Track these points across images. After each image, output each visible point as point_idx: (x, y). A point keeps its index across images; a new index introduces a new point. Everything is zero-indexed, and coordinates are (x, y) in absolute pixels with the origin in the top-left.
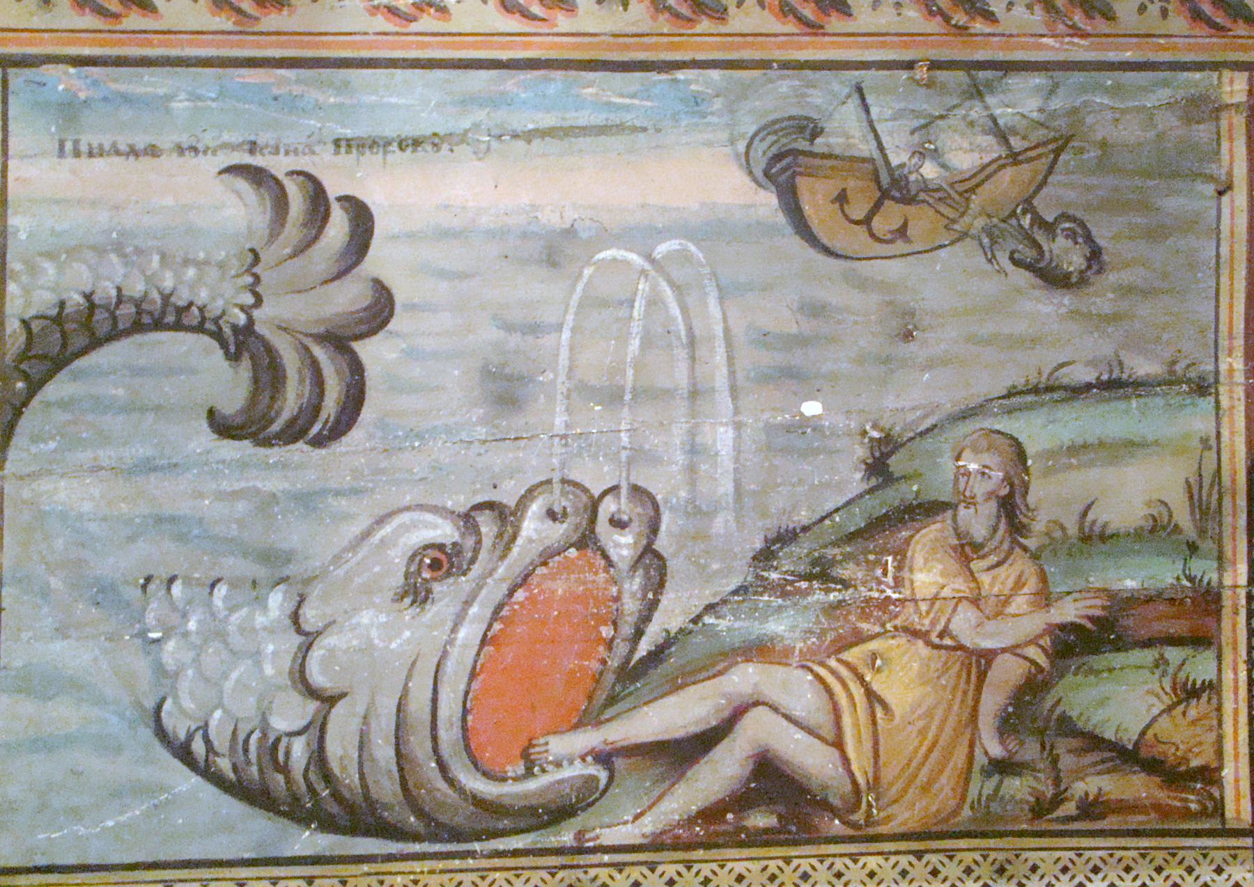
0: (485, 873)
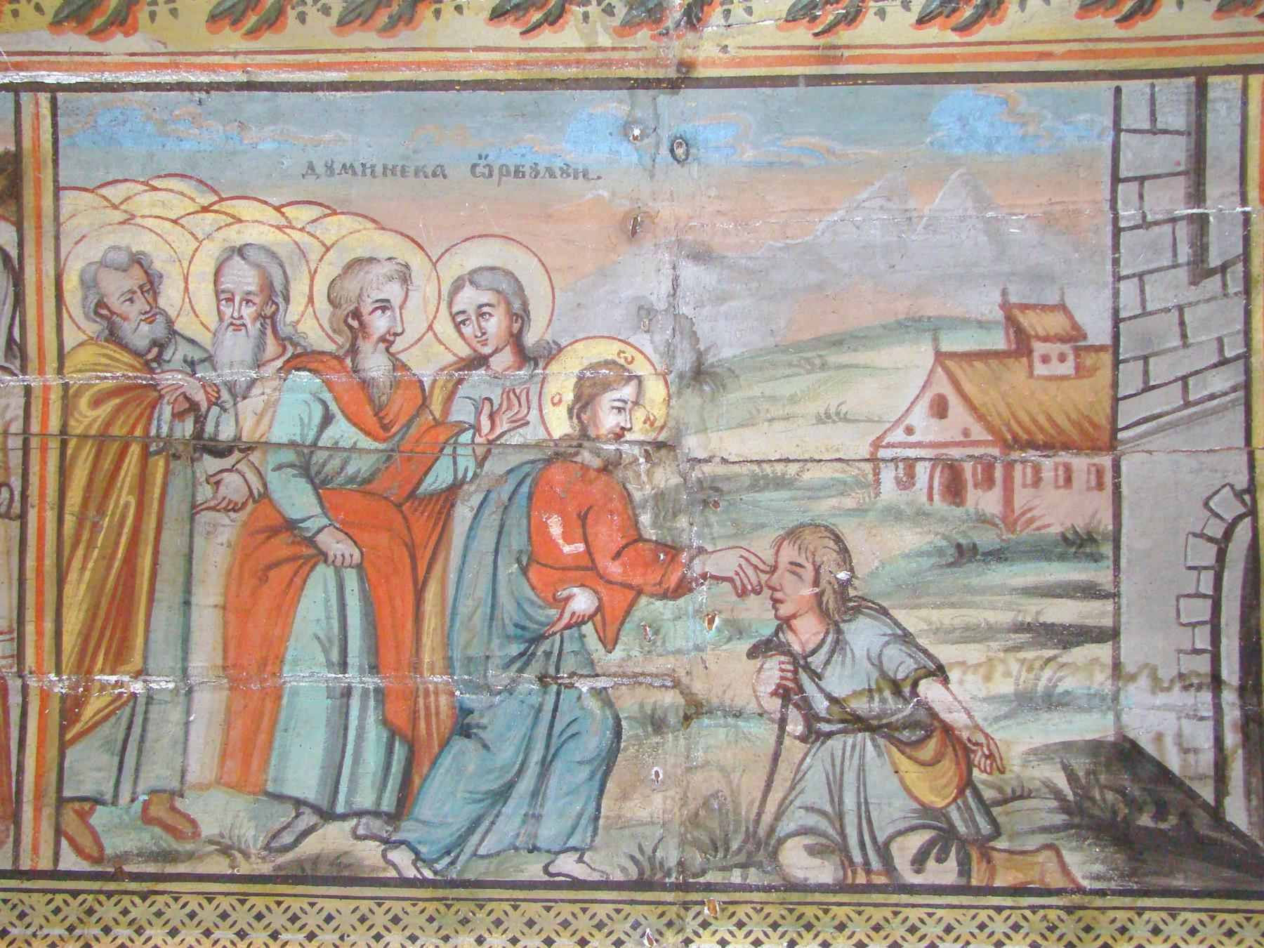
0: (620, 906)
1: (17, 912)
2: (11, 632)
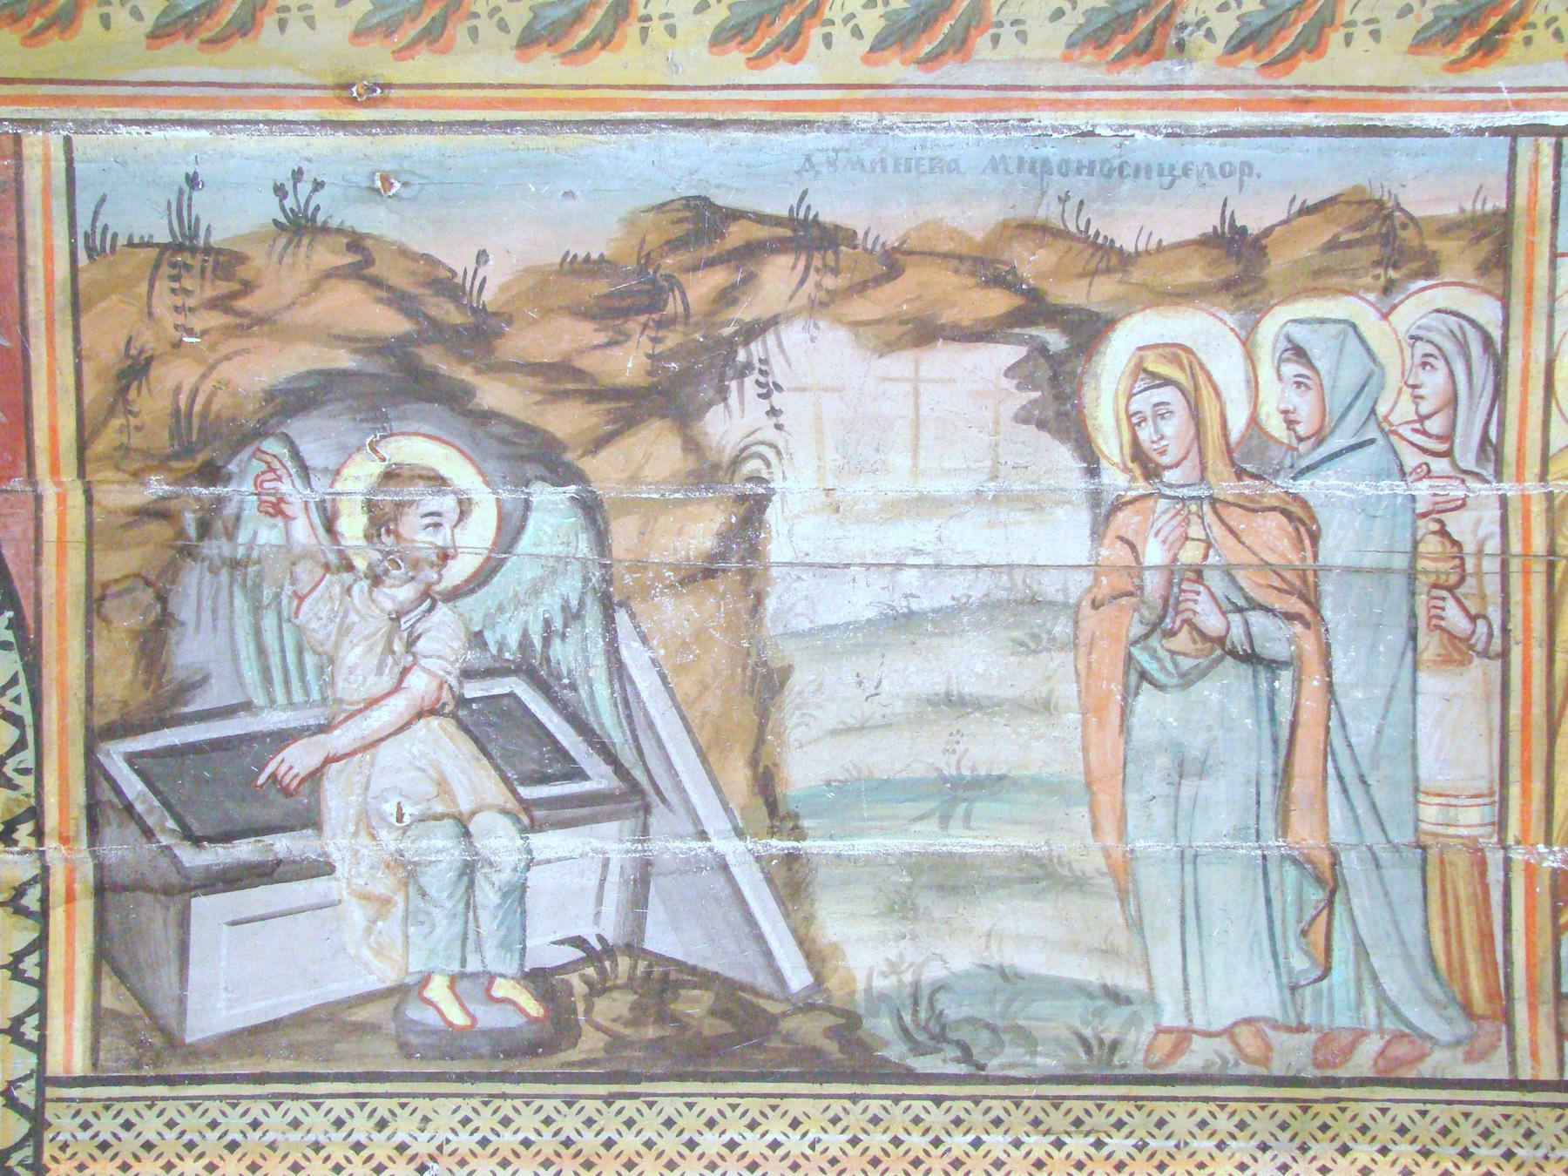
0: (1387, 1105)
1: (1521, 1130)
2: (1491, 794)
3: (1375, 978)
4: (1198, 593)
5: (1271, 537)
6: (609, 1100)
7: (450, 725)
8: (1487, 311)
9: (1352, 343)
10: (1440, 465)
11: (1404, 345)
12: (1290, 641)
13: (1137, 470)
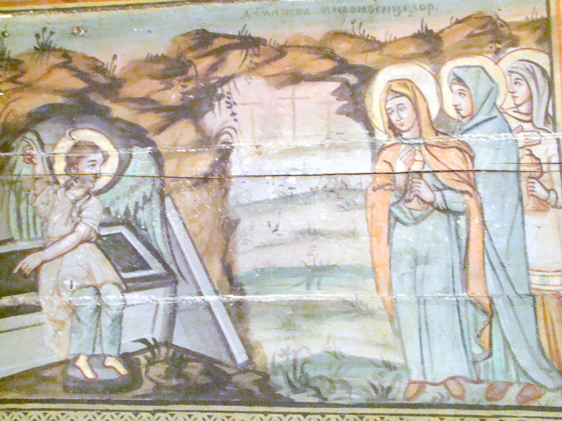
3: (514, 358)
4: (420, 183)
5: (453, 159)
6: (153, 413)
7: (93, 246)
8: (542, 59)
9: (483, 75)
10: (527, 126)
11: (506, 75)
12: (464, 203)
13: (391, 133)
